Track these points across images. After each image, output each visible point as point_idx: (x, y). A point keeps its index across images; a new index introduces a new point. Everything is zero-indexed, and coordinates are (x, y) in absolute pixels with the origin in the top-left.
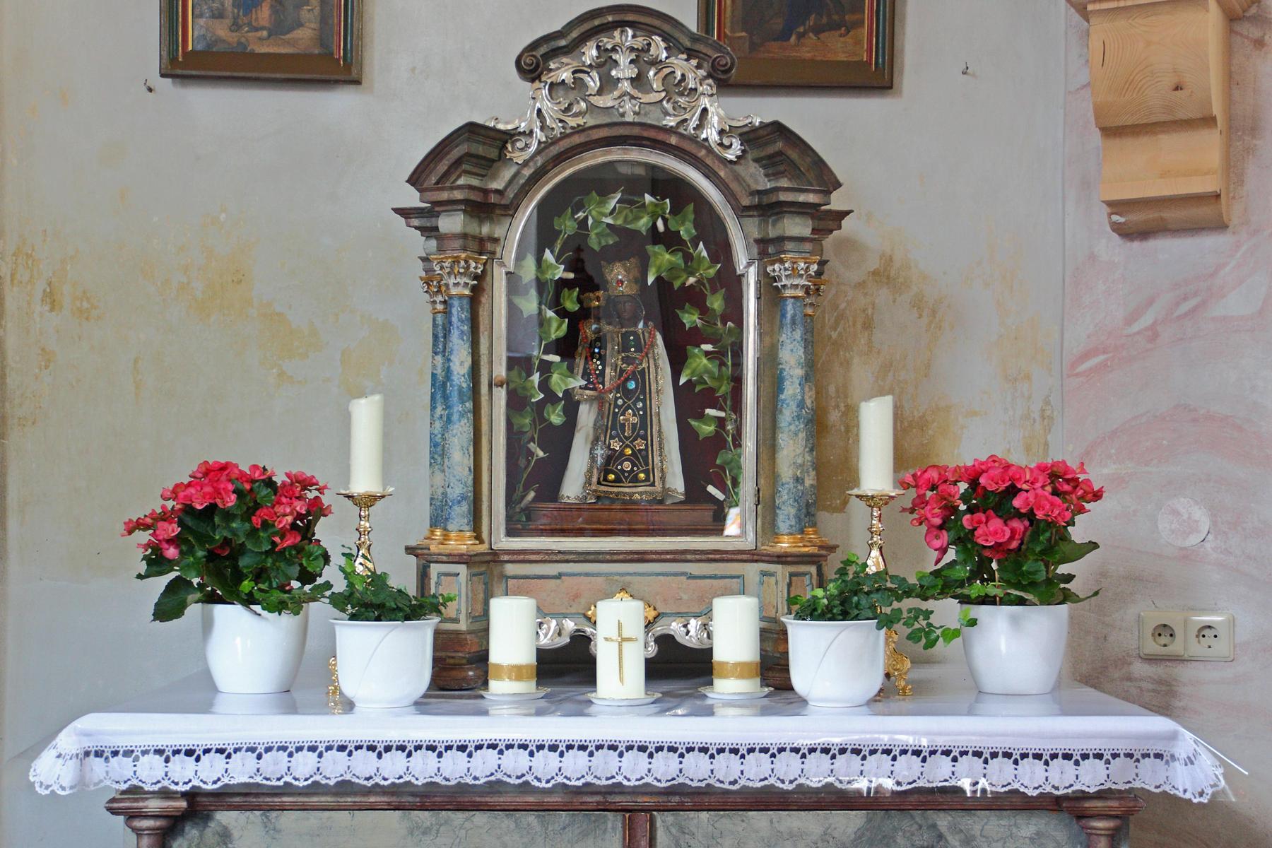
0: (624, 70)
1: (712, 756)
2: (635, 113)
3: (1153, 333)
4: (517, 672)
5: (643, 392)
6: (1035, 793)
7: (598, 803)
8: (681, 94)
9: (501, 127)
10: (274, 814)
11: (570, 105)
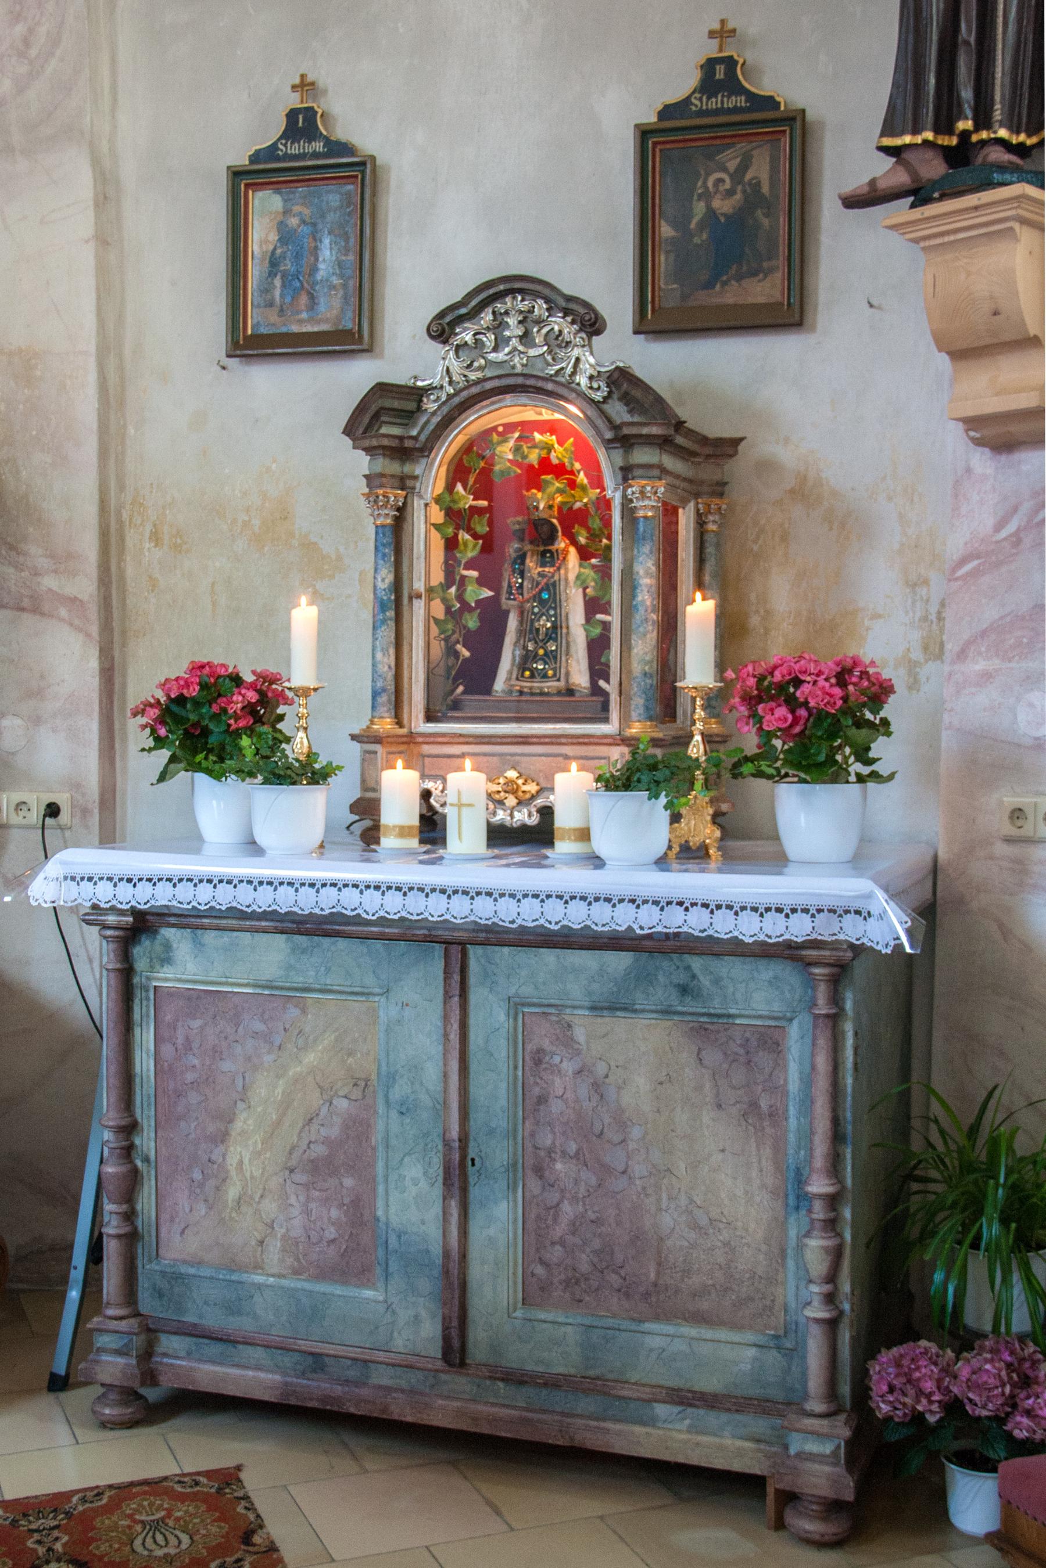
0: (513, 328)
1: (472, 898)
2: (523, 365)
3: (1016, 539)
4: (403, 832)
5: (555, 601)
6: (751, 940)
7: (425, 935)
8: (559, 346)
9: (420, 384)
10: (199, 932)
11: (472, 362)
